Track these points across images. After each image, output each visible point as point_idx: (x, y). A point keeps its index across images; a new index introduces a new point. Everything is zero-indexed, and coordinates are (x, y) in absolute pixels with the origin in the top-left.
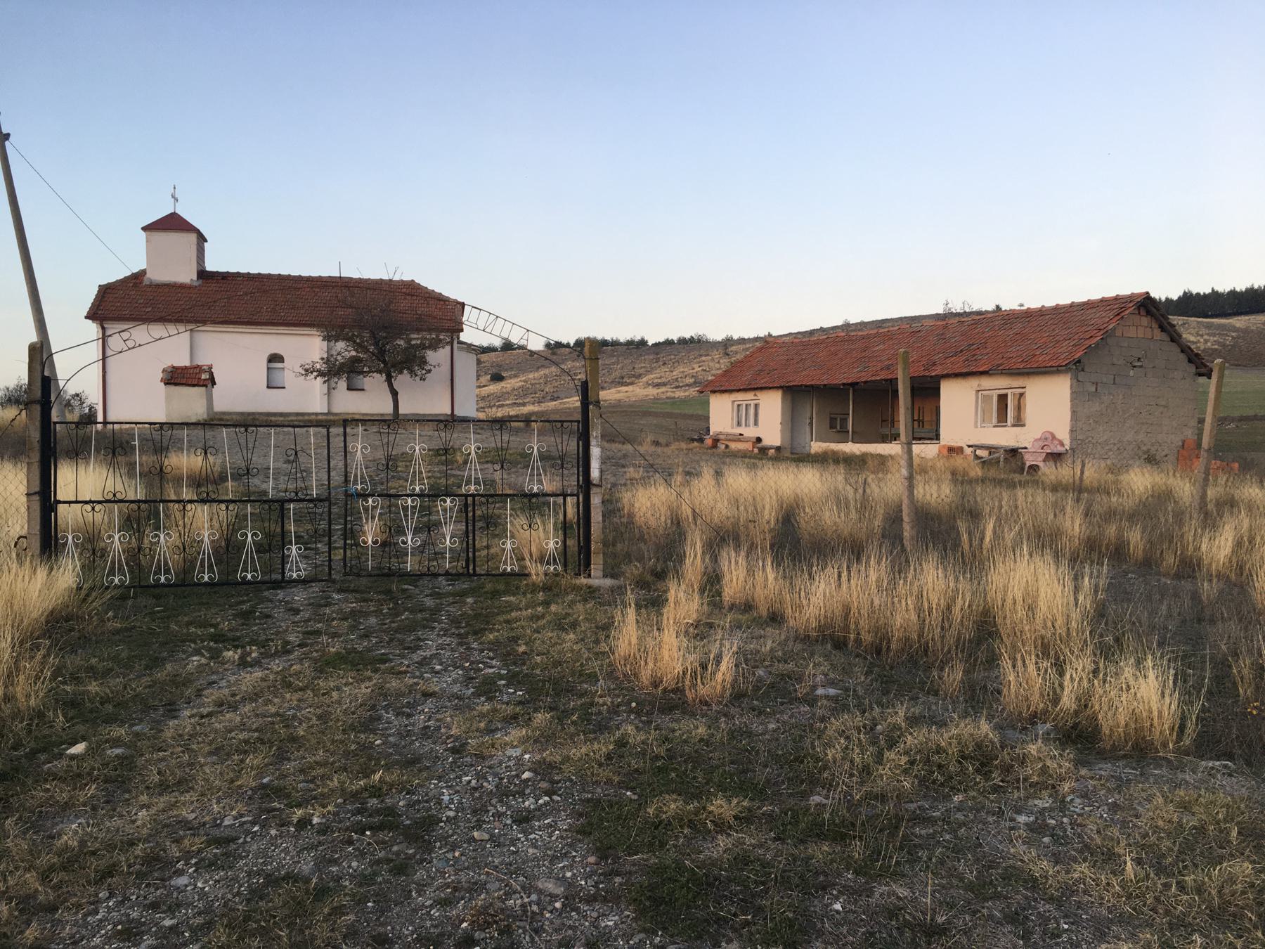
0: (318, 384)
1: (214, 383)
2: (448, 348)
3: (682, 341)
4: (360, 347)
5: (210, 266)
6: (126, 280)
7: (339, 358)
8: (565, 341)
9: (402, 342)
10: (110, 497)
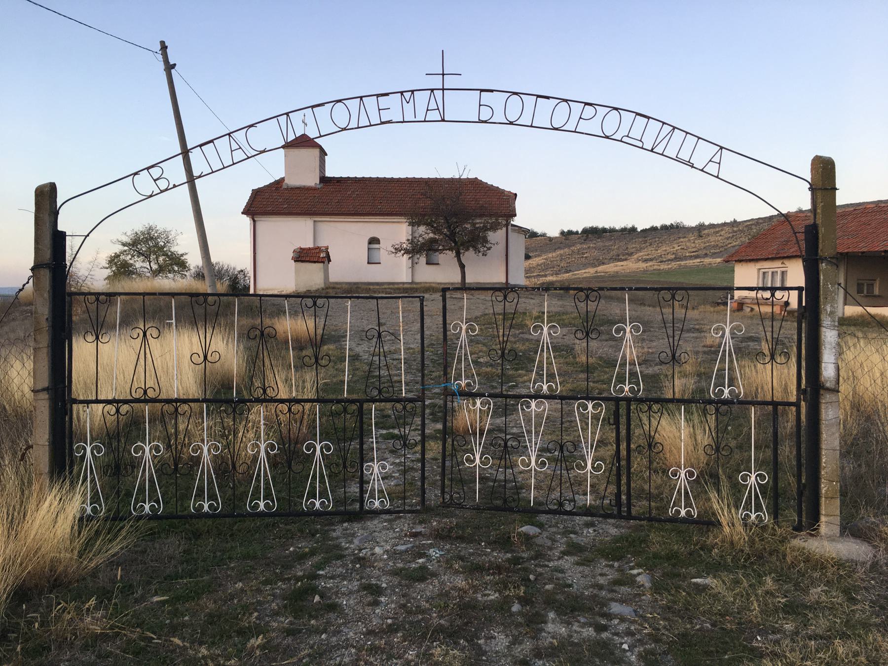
0: (404, 260)
1: (329, 260)
2: (504, 229)
3: (664, 228)
4: (436, 230)
5: (329, 174)
7: (421, 239)
8: (574, 230)
9: (468, 226)
10: (138, 395)
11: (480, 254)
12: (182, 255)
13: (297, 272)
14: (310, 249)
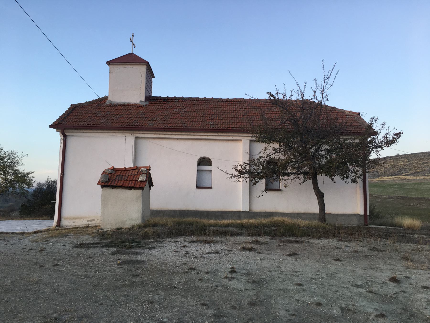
0: (241, 186)
5: (155, 93)
6: (93, 102)
11: (349, 180)
12: (27, 174)
13: (104, 202)
14: (125, 170)
